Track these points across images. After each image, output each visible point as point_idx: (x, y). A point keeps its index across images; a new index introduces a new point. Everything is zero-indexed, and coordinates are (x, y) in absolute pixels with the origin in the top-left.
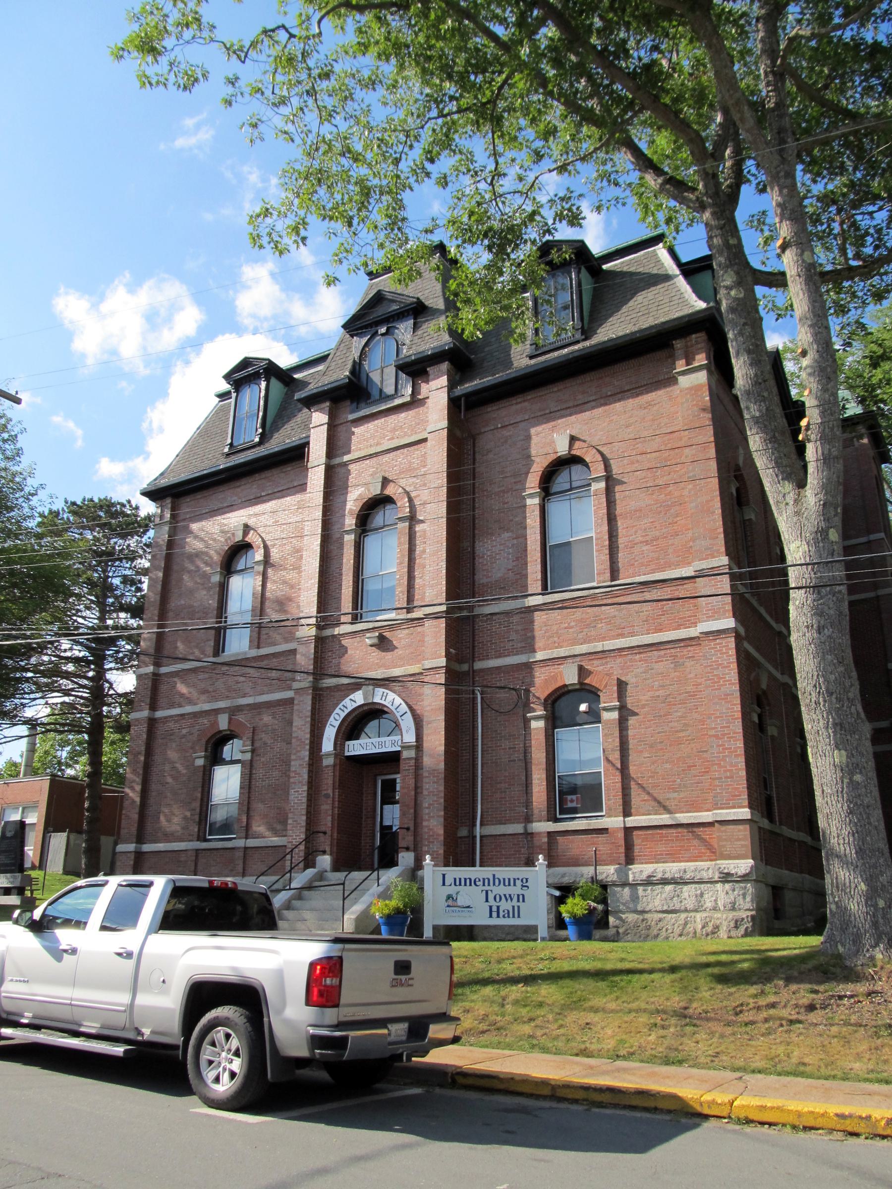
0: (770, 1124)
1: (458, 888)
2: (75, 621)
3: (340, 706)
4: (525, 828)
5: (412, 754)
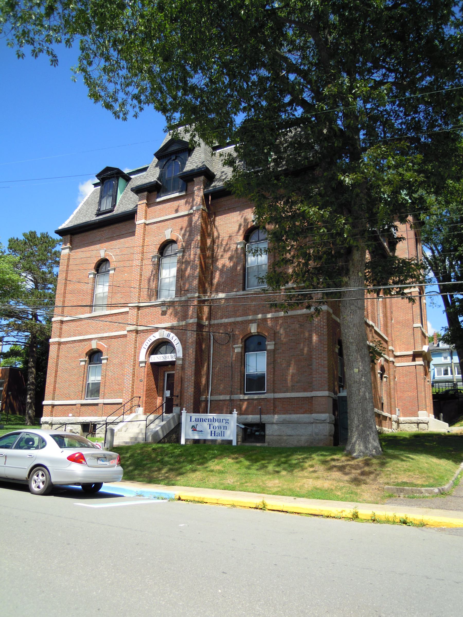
0: (298, 513)
1: (197, 423)
2: (309, 307)
3: (148, 339)
4: (230, 397)
5: (180, 362)
